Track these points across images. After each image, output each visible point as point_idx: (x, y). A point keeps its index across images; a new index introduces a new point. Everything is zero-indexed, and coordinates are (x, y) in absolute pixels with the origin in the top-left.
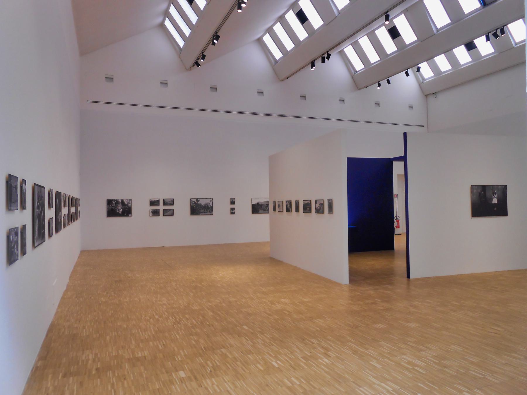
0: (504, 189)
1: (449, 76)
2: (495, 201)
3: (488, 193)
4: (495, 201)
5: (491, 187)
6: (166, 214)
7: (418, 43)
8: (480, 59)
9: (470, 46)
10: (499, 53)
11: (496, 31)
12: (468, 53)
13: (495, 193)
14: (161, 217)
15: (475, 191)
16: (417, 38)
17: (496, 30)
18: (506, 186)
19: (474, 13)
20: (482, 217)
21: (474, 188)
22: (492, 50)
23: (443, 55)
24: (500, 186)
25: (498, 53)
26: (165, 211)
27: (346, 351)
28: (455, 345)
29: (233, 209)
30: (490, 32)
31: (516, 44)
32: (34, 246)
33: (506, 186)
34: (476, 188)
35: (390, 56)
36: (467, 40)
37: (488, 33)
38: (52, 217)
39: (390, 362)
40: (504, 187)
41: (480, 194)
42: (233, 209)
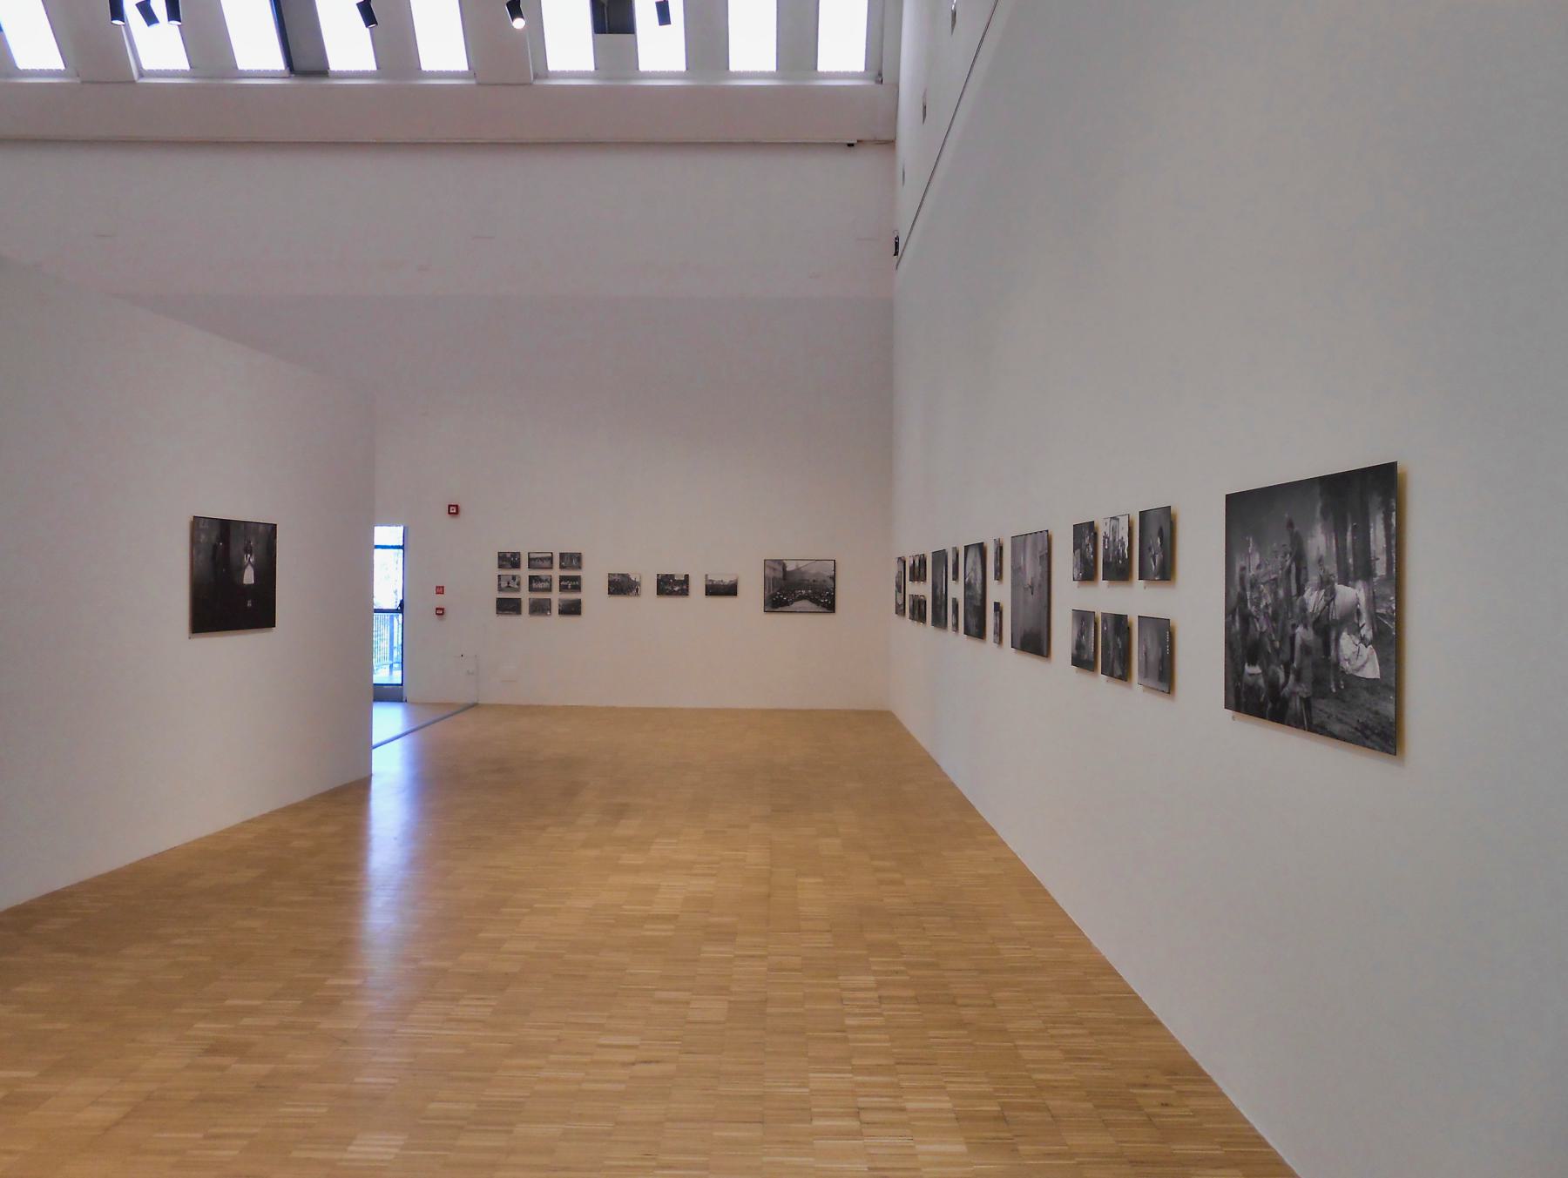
1: (663, 98)
2: (249, 577)
3: (236, 548)
4: (249, 577)
5: (242, 527)
6: (1045, 654)
8: (8, 75)
12: (594, 40)
15: (203, 538)
21: (201, 526)
22: (461, 65)
24: (261, 528)
25: (78, 81)
26: (516, 565)
28: (819, 1144)
29: (714, 590)
31: (142, 74)
34: (206, 526)
38: (727, 580)
40: (270, 528)
41: (215, 547)
42: (714, 590)
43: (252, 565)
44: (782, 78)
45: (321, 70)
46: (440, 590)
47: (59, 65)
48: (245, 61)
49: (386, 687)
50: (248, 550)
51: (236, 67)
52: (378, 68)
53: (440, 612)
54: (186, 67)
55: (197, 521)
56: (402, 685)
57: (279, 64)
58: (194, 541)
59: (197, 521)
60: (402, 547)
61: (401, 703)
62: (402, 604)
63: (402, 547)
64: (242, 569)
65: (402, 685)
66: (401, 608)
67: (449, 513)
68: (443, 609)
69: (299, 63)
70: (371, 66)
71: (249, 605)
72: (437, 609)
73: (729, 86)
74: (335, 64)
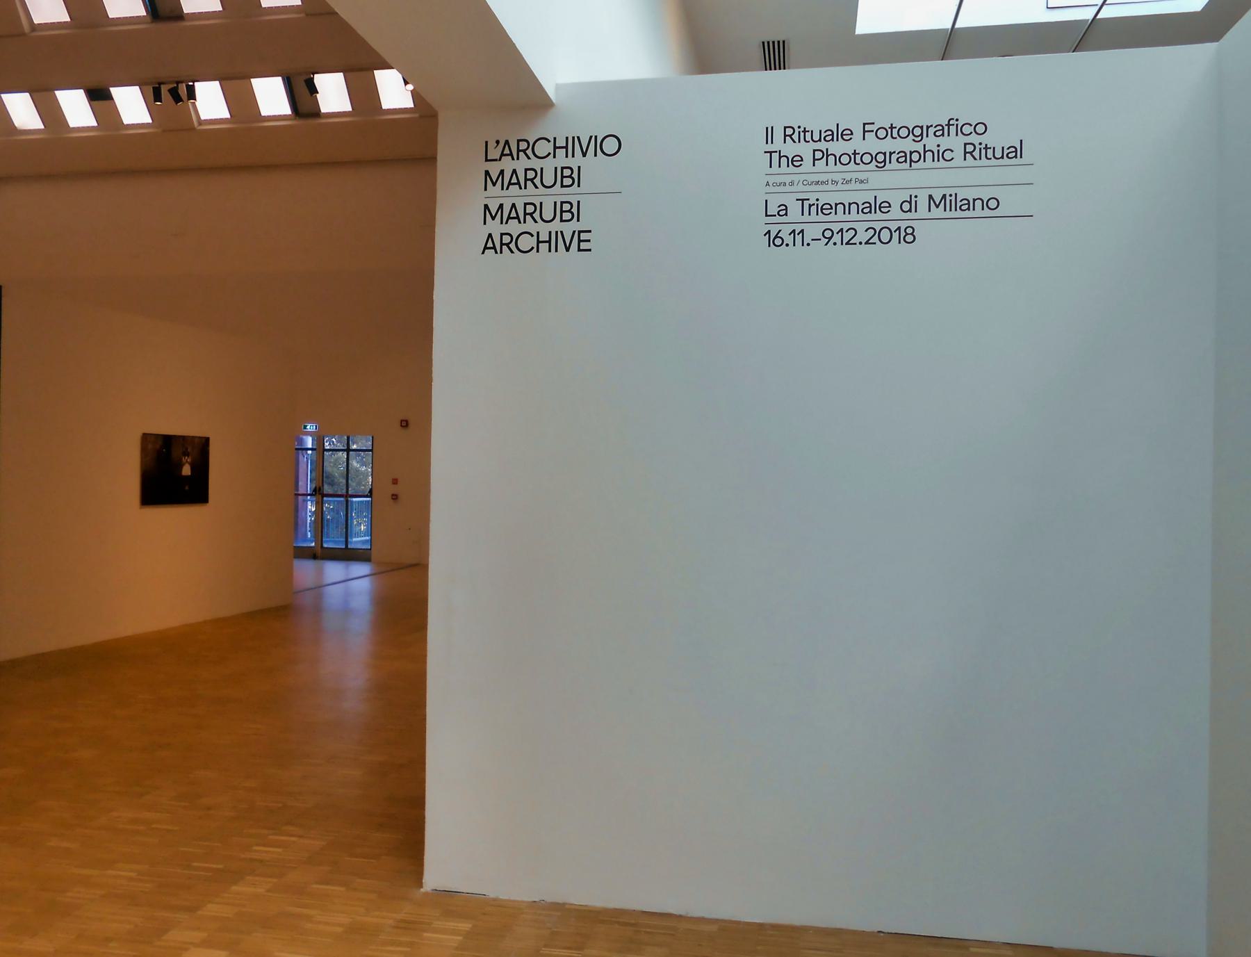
0: (203, 446)
2: (186, 470)
3: (176, 452)
4: (186, 470)
7: (224, 21)
9: (99, 96)
10: (421, 117)
11: (175, 85)
13: (188, 453)
14: (760, 224)
15: (150, 446)
16: (70, 18)
17: (178, 83)
18: (207, 440)
19: (135, 24)
20: (201, 504)
23: (341, 75)
27: (327, 924)
30: (163, 83)
31: (201, 122)
32: (1088, 20)
33: (207, 440)
35: (116, 25)
36: (94, 83)
37: (160, 84)
39: (655, 923)
43: (189, 464)
44: (234, 123)
45: (316, 113)
46: (395, 482)
47: (225, 114)
48: (127, 119)
49: (361, 551)
50: (186, 454)
51: (320, 111)
52: (415, 106)
53: (395, 497)
54: (227, 115)
55: (145, 437)
56: (370, 549)
57: (286, 110)
58: (144, 450)
59: (145, 437)
60: (371, 450)
61: (368, 563)
62: (371, 491)
63: (371, 450)
64: (181, 466)
65: (370, 549)
66: (370, 494)
67: (401, 426)
68: (396, 495)
69: (302, 109)
70: (348, 108)
71: (187, 488)
72: (393, 495)
73: (72, 138)
74: (324, 108)
